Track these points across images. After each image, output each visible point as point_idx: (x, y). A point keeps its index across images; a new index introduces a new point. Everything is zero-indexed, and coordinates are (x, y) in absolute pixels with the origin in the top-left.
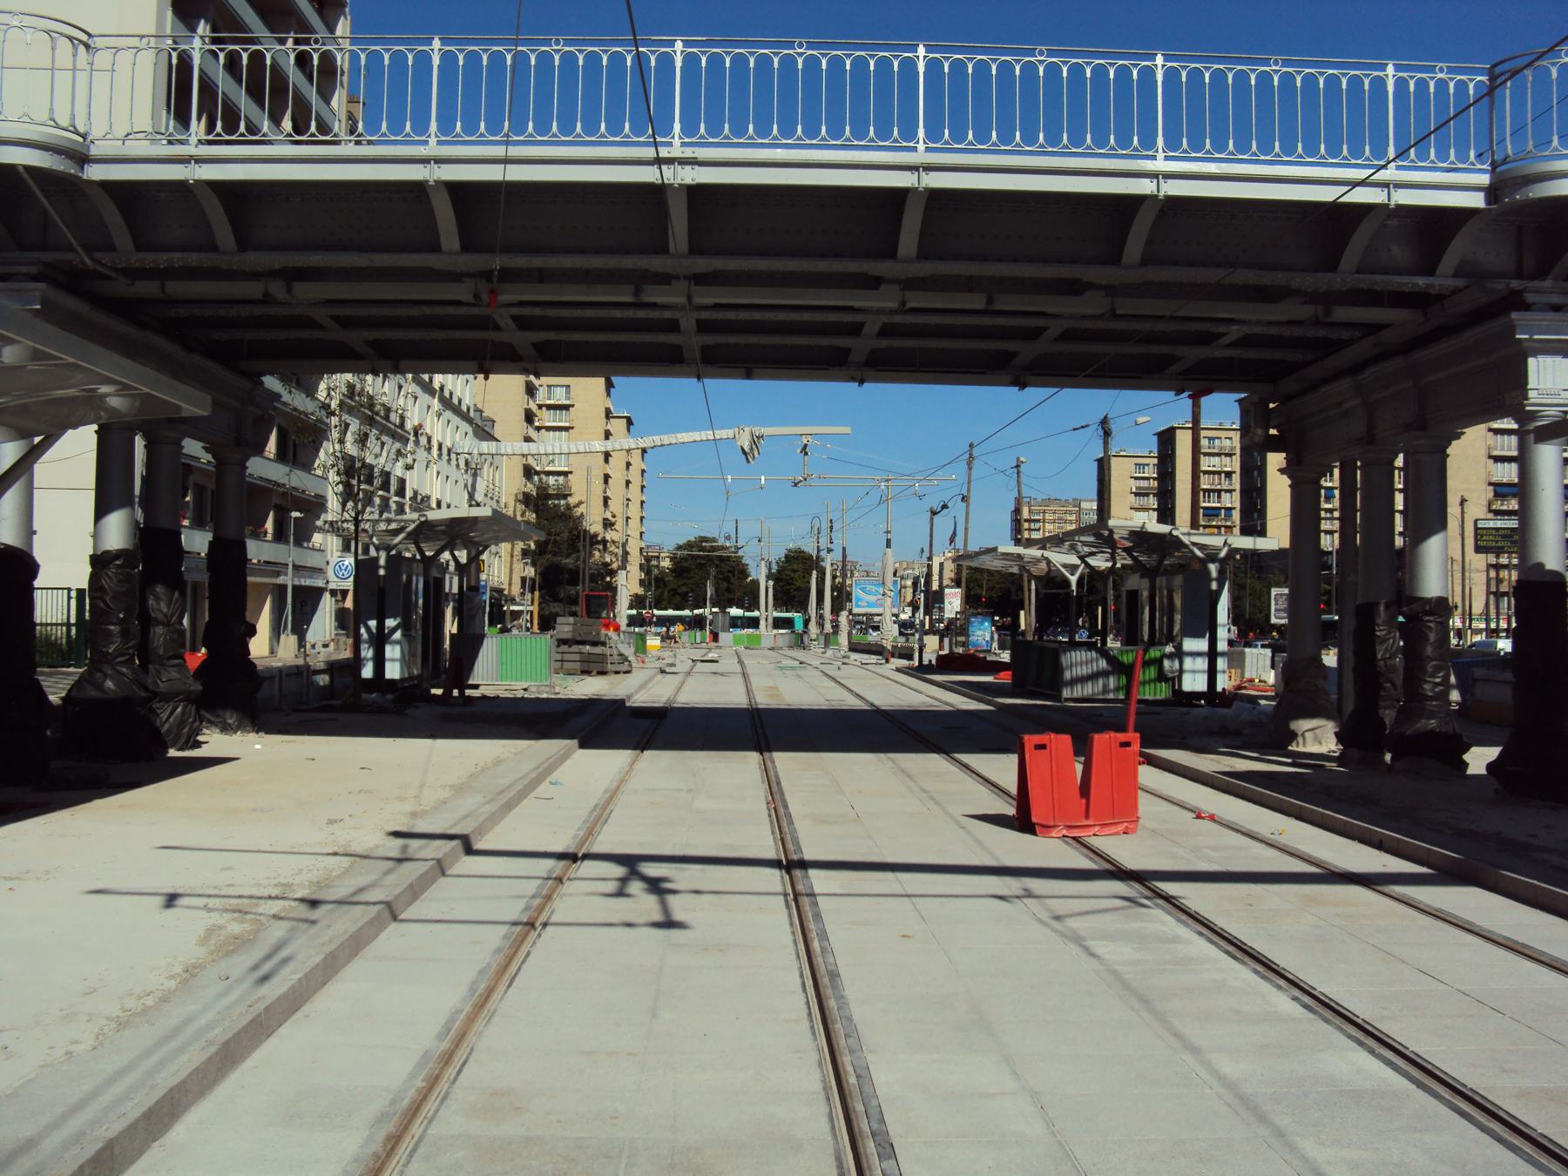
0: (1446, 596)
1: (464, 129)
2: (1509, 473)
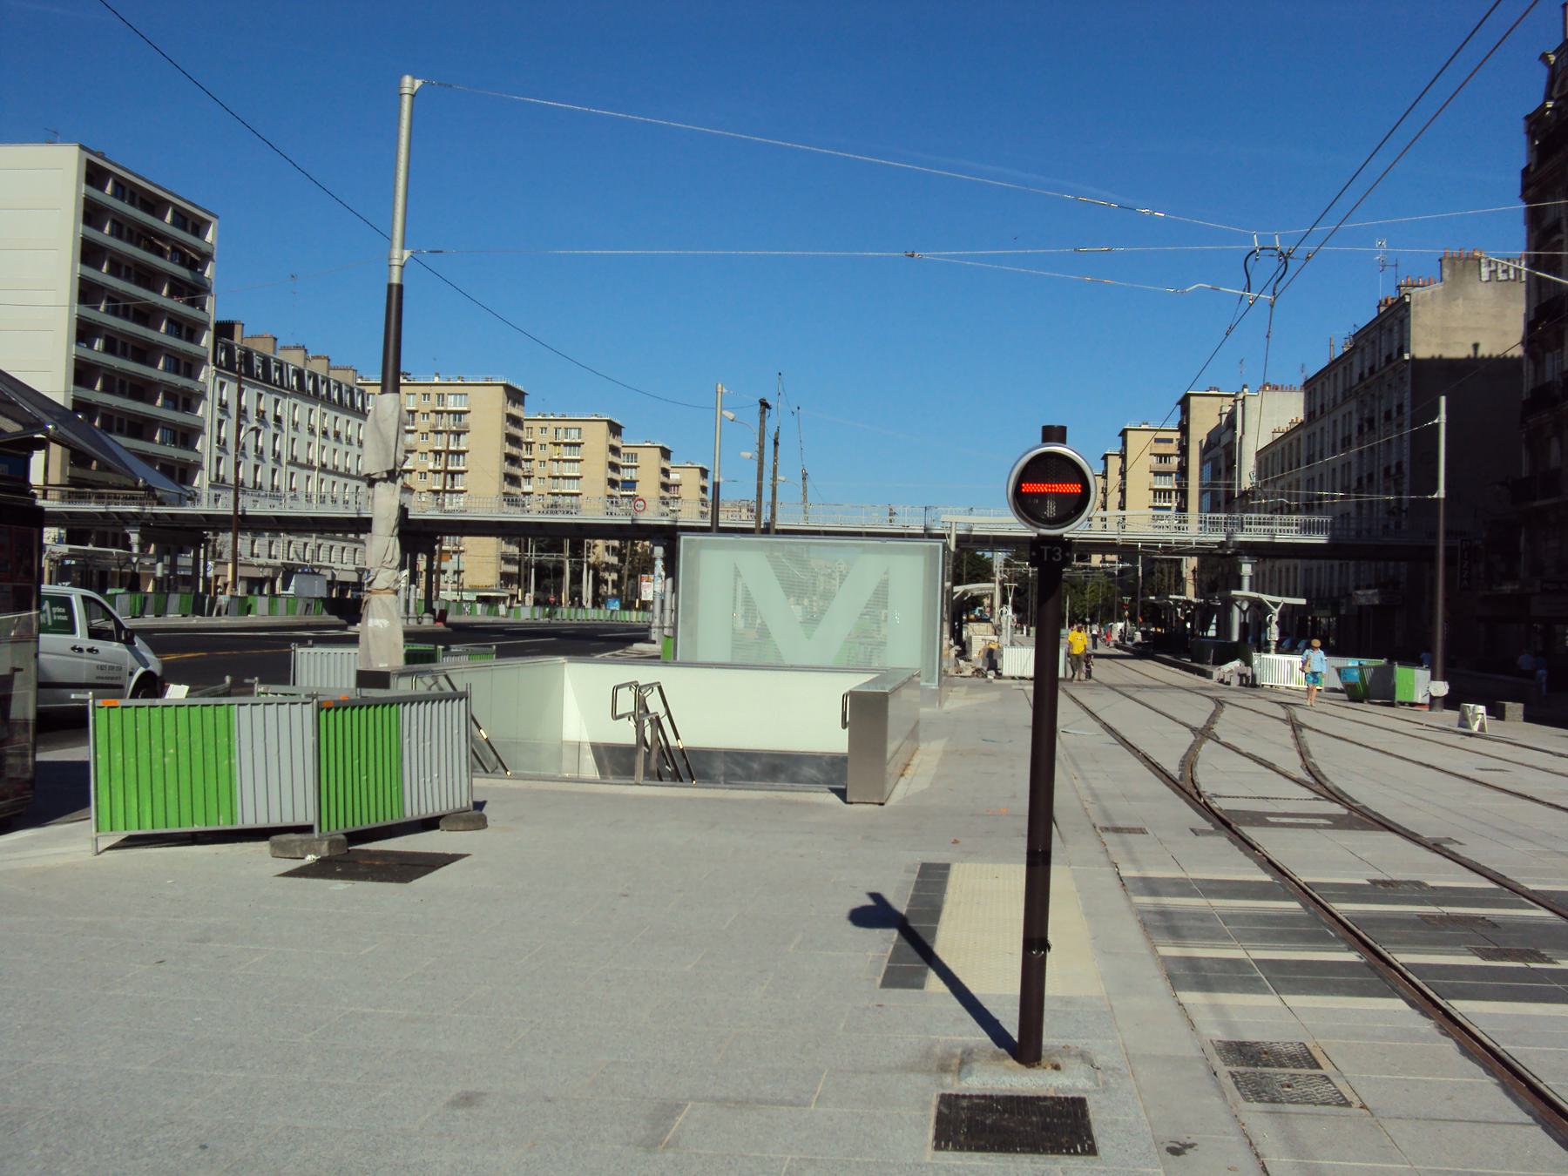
0: (86, 759)
2: (1169, 483)
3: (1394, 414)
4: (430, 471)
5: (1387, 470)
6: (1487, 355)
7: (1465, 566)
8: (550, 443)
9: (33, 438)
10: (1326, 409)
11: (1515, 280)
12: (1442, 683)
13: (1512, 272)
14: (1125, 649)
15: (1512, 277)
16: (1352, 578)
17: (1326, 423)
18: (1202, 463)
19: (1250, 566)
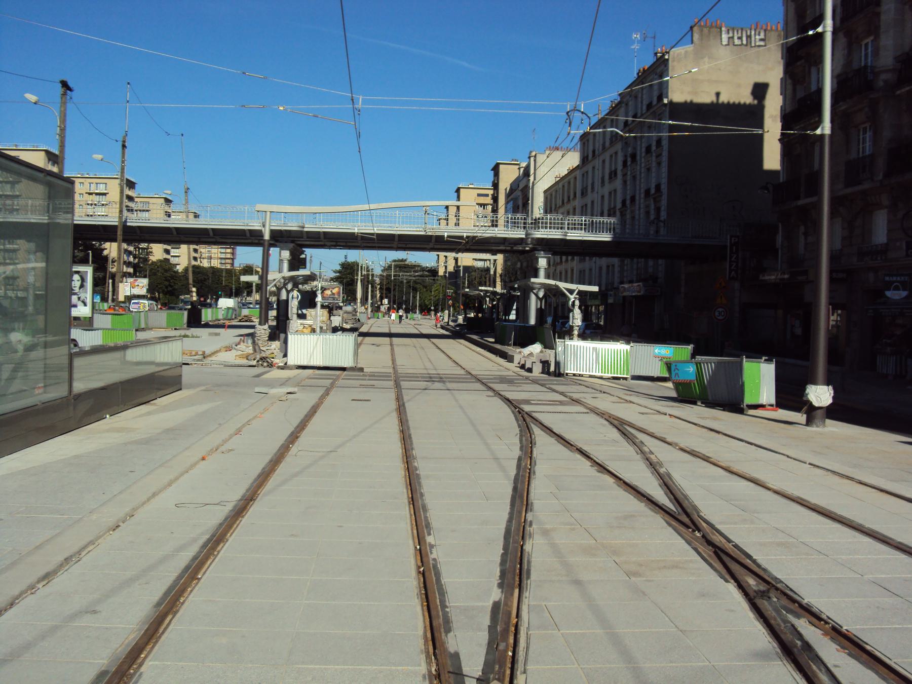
3: (654, 148)
5: (647, 192)
6: (726, 101)
7: (733, 259)
8: (86, 193)
10: (597, 153)
11: (746, 45)
12: (826, 387)
13: (744, 39)
14: (447, 330)
15: (745, 42)
16: (617, 275)
17: (597, 163)
18: (507, 203)
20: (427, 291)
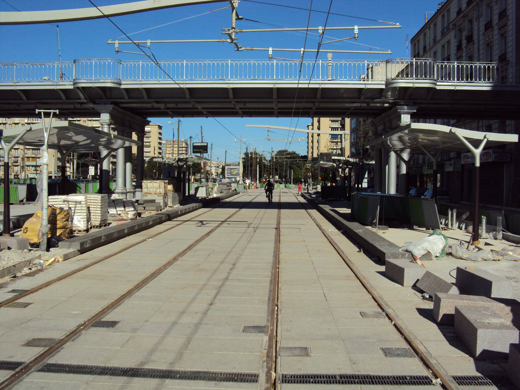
1: (488, 80)
4: (26, 123)
9: (90, 146)
10: (428, 48)
19: (409, 116)
20: (300, 169)
